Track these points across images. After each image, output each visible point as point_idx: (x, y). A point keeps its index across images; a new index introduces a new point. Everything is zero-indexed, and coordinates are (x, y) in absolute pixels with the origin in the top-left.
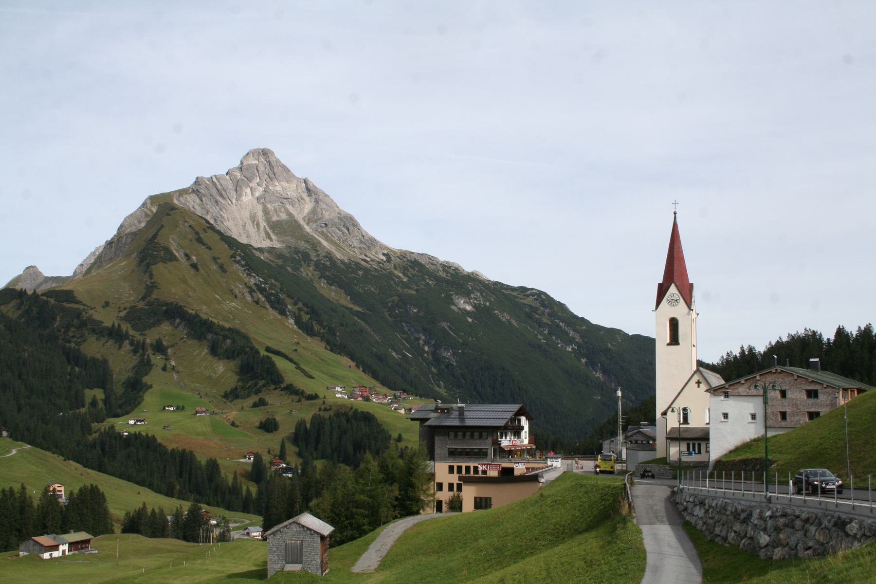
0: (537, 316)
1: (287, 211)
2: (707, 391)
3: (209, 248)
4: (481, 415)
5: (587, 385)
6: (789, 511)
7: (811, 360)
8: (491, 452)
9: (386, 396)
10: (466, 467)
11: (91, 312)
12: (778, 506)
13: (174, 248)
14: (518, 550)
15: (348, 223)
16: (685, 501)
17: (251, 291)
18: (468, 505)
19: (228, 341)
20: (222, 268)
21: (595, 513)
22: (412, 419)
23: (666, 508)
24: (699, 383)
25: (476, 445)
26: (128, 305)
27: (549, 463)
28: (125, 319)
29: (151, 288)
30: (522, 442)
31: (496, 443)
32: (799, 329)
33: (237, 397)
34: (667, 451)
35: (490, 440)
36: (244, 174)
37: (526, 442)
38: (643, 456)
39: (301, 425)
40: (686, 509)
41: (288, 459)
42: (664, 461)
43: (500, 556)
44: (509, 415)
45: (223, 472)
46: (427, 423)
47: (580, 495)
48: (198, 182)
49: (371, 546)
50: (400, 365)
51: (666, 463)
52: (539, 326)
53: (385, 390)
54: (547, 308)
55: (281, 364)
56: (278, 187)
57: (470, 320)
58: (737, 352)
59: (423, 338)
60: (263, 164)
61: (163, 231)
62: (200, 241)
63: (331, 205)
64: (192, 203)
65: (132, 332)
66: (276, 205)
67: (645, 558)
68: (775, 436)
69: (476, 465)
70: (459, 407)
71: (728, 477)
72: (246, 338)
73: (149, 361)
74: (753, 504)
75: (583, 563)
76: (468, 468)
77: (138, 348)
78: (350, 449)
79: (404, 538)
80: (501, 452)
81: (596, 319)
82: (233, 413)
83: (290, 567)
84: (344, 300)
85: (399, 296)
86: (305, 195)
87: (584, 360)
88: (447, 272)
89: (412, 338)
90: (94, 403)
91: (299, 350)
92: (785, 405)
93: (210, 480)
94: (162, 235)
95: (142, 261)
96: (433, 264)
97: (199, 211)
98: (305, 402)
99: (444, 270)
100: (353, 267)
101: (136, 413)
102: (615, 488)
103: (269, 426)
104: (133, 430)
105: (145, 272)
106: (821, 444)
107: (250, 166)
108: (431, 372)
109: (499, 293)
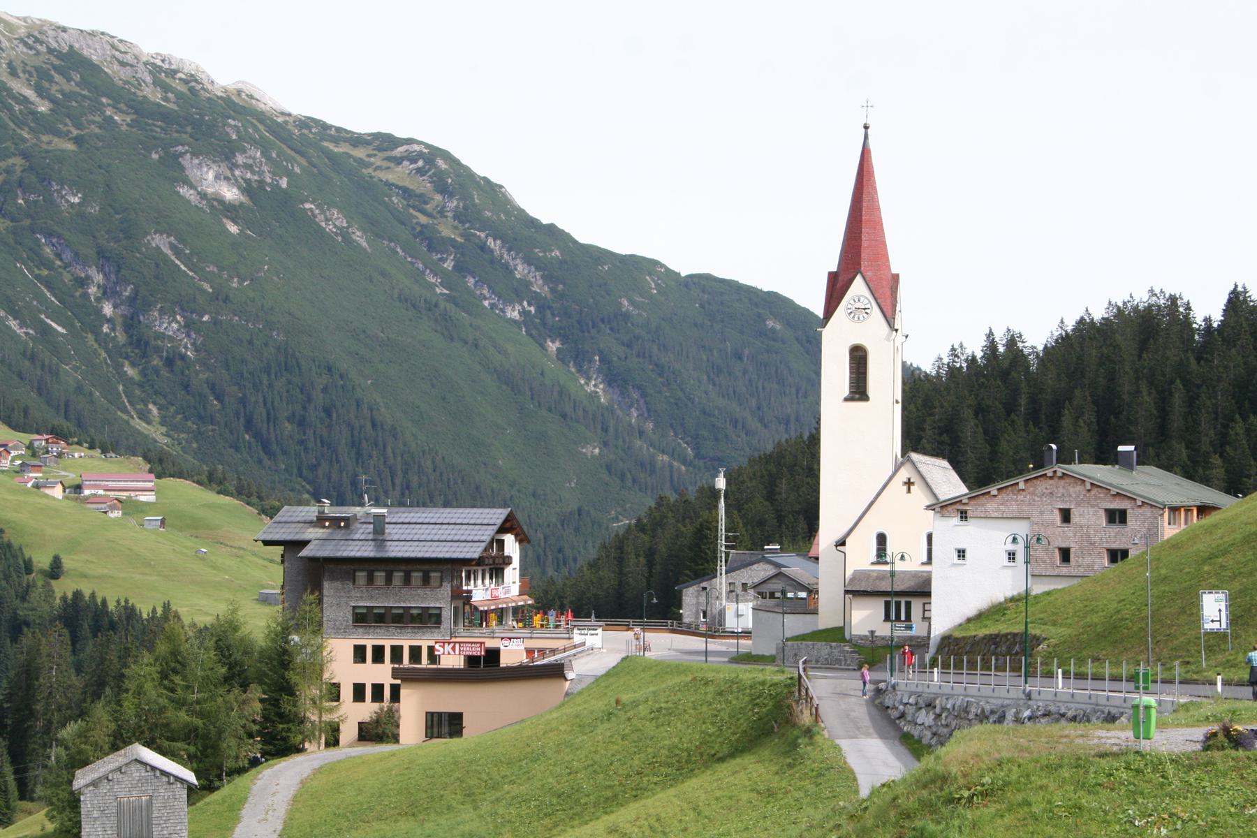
0: (423, 219)
2: (928, 507)
4: (421, 532)
5: (564, 416)
6: (1053, 708)
7: (1121, 448)
8: (448, 615)
10: (411, 648)
12: (1040, 704)
14: (609, 793)
16: (901, 703)
21: (744, 727)
22: (267, 543)
23: (869, 714)
24: (909, 483)
25: (417, 599)
27: (577, 637)
30: (508, 591)
32: (1134, 289)
35: (447, 589)
38: (795, 624)
40: (902, 716)
42: (836, 634)
43: (570, 804)
44: (487, 534)
46: (305, 552)
47: (709, 697)
49: (243, 812)
50: (32, 358)
51: (843, 640)
52: (431, 248)
54: (451, 195)
57: (233, 229)
58: (976, 347)
59: (99, 278)
67: (855, 779)
68: (1048, 593)
69: (432, 643)
70: (376, 516)
71: (958, 666)
74: (1007, 702)
79: (305, 796)
81: (589, 229)
85: (25, 155)
87: (553, 346)
88: (166, 88)
89: (67, 277)
96: (123, 64)
99: (157, 83)
102: (775, 685)
106: (1118, 612)
108: (122, 376)
109: (312, 147)
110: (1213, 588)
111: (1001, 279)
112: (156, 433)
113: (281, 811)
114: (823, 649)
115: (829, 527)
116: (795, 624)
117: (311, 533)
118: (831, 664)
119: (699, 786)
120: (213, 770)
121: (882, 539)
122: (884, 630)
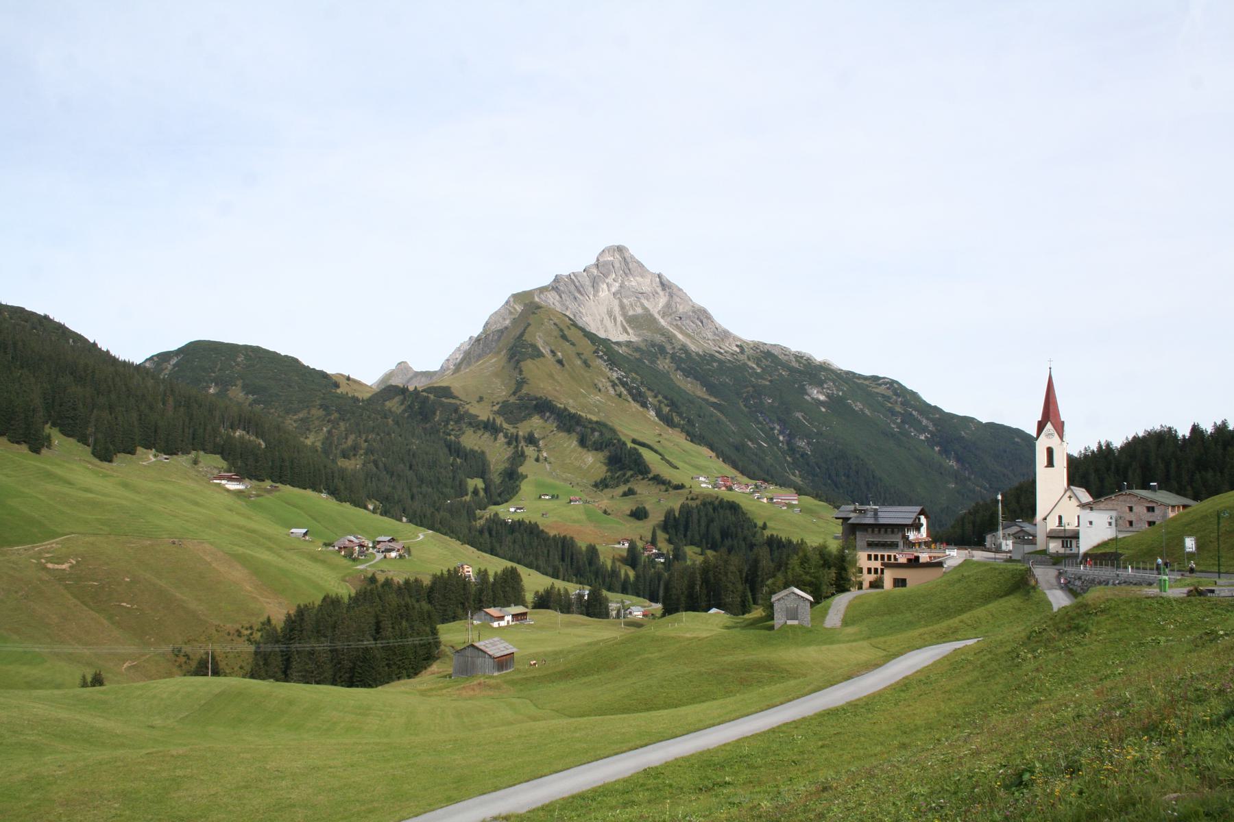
1: (642, 305)
3: (573, 344)
4: (890, 515)
8: (901, 544)
9: (747, 486)
11: (467, 406)
13: (540, 344)
15: (702, 316)
17: (614, 385)
19: (597, 434)
20: (586, 364)
25: (889, 538)
26: (500, 400)
27: (947, 552)
29: (521, 383)
32: (1156, 425)
33: (606, 486)
34: (1047, 545)
35: (900, 535)
36: (600, 271)
37: (925, 535)
38: (1028, 548)
39: (669, 513)
41: (659, 545)
42: (1044, 552)
44: (915, 515)
48: (557, 279)
53: (745, 480)
55: (647, 455)
56: (633, 282)
58: (1094, 447)
61: (530, 329)
62: (564, 337)
63: (685, 299)
64: (552, 299)
65: (505, 425)
72: (613, 431)
73: (523, 452)
75: (746, 752)
76: (889, 557)
77: (512, 440)
78: (718, 536)
79: (850, 606)
80: (910, 544)
82: (604, 500)
83: (789, 622)
84: (701, 392)
86: (659, 290)
87: (937, 449)
90: (476, 492)
91: (663, 441)
92: (1132, 517)
94: (525, 332)
95: (511, 358)
97: (559, 308)
98: (673, 492)
100: (709, 358)
101: (515, 500)
103: (639, 514)
104: (516, 518)
105: (515, 368)
107: (606, 263)
112: (798, 480)
114: (1039, 557)
115: (1039, 515)
117: (852, 515)
118: (1042, 563)
120: (819, 597)
121: (1060, 518)
122: (1062, 551)
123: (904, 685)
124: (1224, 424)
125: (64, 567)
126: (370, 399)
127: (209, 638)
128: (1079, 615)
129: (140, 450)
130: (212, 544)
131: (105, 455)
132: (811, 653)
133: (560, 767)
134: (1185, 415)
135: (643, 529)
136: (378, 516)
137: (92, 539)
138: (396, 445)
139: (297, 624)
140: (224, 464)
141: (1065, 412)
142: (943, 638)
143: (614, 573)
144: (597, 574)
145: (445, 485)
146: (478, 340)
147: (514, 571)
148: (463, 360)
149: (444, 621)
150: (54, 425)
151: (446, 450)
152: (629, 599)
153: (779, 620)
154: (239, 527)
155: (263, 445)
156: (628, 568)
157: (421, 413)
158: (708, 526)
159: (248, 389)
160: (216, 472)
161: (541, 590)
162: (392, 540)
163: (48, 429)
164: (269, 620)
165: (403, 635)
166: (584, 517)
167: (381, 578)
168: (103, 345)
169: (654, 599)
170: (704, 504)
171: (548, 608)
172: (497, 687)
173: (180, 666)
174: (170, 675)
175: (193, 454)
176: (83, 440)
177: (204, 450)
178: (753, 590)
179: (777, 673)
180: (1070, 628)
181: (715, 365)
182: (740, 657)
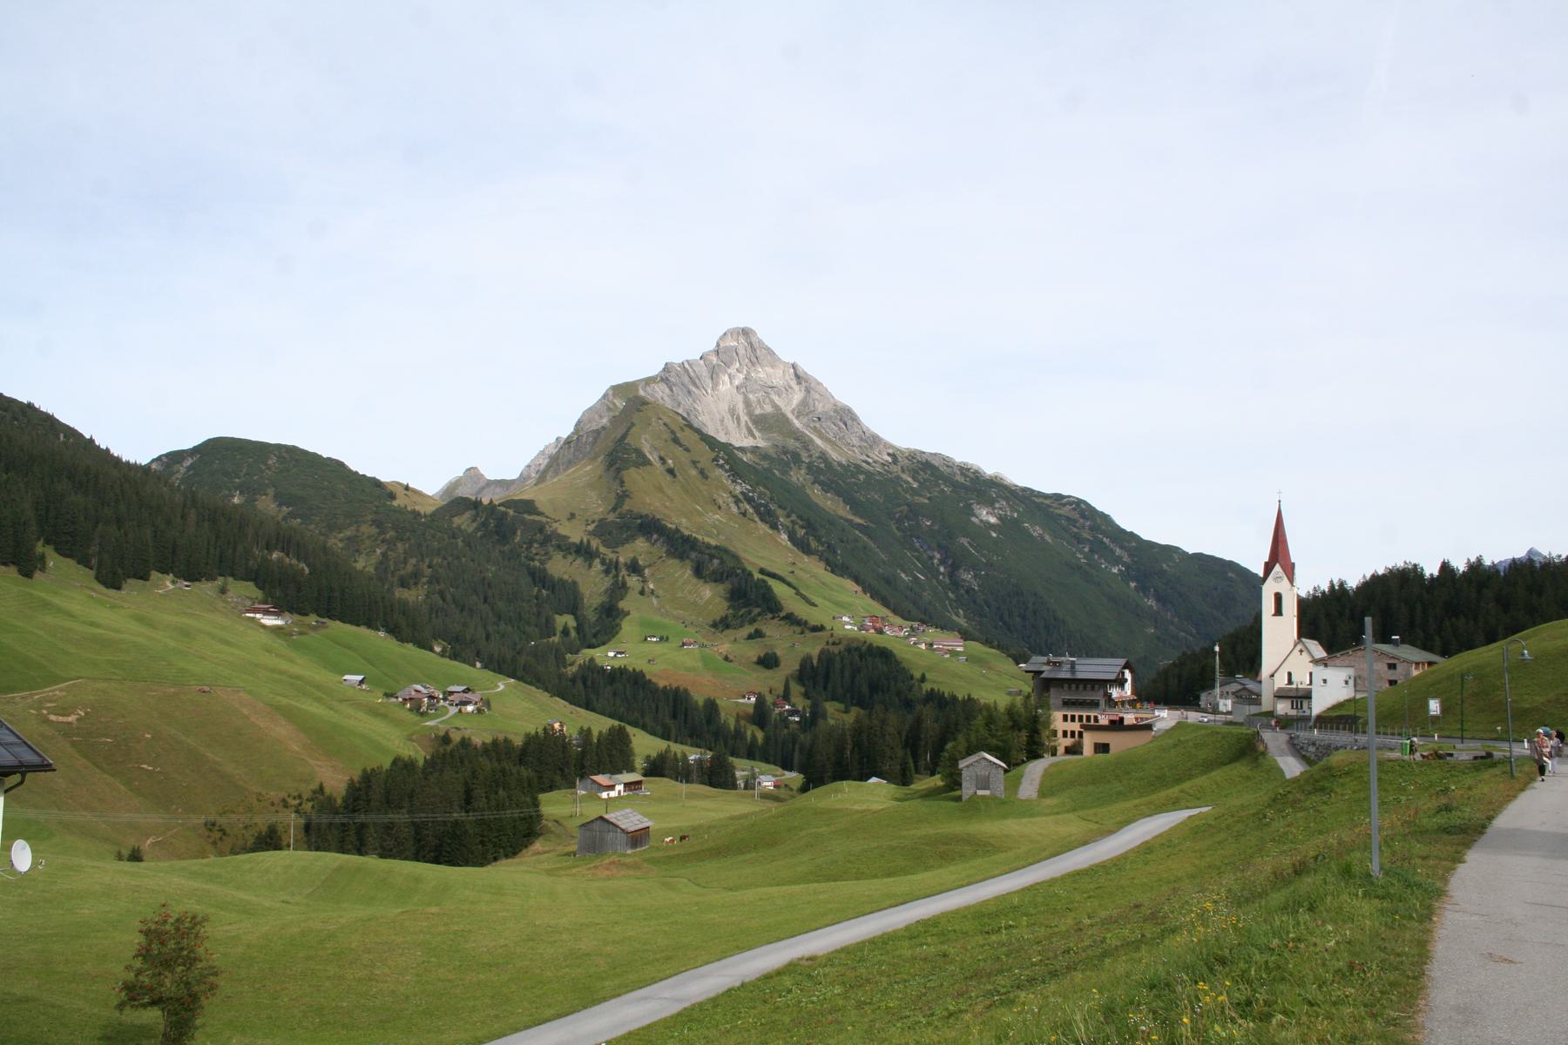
1: (772, 402)
3: (687, 450)
4: (1089, 668)
8: (1102, 702)
9: (901, 628)
11: (555, 525)
15: (845, 417)
17: (737, 502)
18: (1088, 749)
19: (716, 561)
26: (596, 517)
28: (593, 533)
29: (623, 497)
31: (1109, 697)
33: (727, 627)
34: (1274, 706)
36: (721, 358)
38: (1254, 709)
39: (805, 663)
41: (793, 700)
42: (1270, 714)
44: (1118, 669)
45: (723, 715)
48: (667, 368)
53: (898, 620)
55: (779, 589)
56: (761, 374)
58: (1325, 587)
60: (743, 347)
62: (676, 441)
63: (825, 395)
64: (660, 393)
65: (602, 549)
66: (759, 395)
72: (736, 558)
73: (624, 584)
76: (1088, 718)
77: (611, 568)
78: (865, 689)
79: (1047, 774)
82: (724, 645)
83: (980, 792)
84: (842, 510)
86: (793, 383)
87: (1133, 585)
90: (565, 632)
93: (709, 722)
94: (627, 434)
95: (610, 465)
97: (669, 404)
98: (809, 634)
103: (768, 662)
104: (617, 664)
107: (728, 349)
110: (1434, 697)
111: (1335, 559)
112: (962, 622)
113: (1038, 781)
114: (1264, 720)
115: (1266, 670)
116: (1254, 709)
117: (1045, 668)
118: (1269, 726)
119: (1217, 774)
120: (1012, 763)
121: (1290, 674)
122: (1293, 712)
123: (1147, 849)
124: (1479, 560)
125: (70, 719)
126: (434, 514)
127: (250, 809)
128: (1324, 778)
129: (155, 575)
130: (250, 692)
131: (112, 581)
132: (1012, 826)
133: (549, 1012)
134: (1440, 541)
135: (773, 680)
136: (447, 661)
137: (104, 685)
138: (460, 573)
139: (363, 792)
140: (258, 594)
141: (1295, 555)
142: (1174, 804)
143: (739, 734)
144: (717, 735)
145: (528, 623)
146: (568, 442)
147: (621, 731)
148: (548, 467)
149: (544, 791)
150: (47, 542)
151: (529, 579)
152: (759, 766)
153: (967, 790)
154: (281, 672)
155: (307, 571)
156: (755, 728)
157: (497, 533)
158: (853, 678)
159: (281, 499)
160: (248, 603)
161: (654, 754)
162: (467, 691)
163: (40, 548)
164: (321, 788)
165: (499, 806)
166: (700, 664)
167: (456, 737)
168: (102, 442)
169: (787, 766)
170: (849, 650)
171: (662, 775)
172: (636, 866)
173: (214, 843)
174: (202, 854)
175: (220, 581)
176: (84, 561)
177: (233, 575)
178: (915, 757)
179: (982, 847)
180: (1316, 790)
181: (862, 477)
182: (927, 830)
